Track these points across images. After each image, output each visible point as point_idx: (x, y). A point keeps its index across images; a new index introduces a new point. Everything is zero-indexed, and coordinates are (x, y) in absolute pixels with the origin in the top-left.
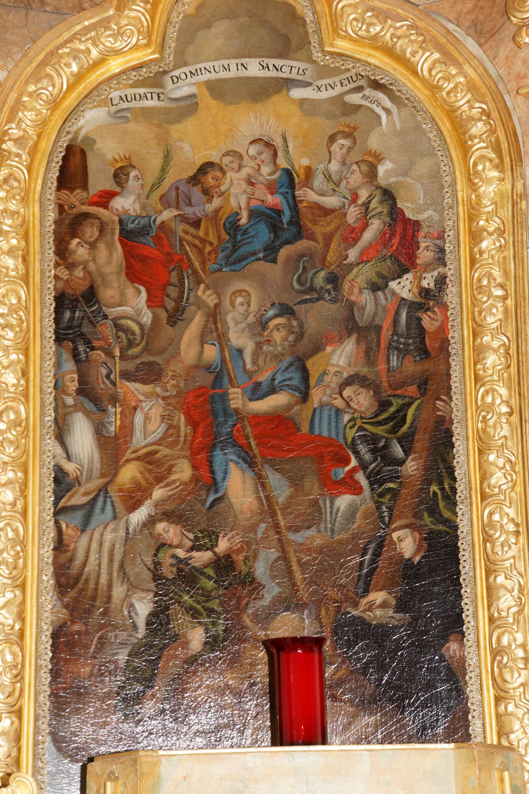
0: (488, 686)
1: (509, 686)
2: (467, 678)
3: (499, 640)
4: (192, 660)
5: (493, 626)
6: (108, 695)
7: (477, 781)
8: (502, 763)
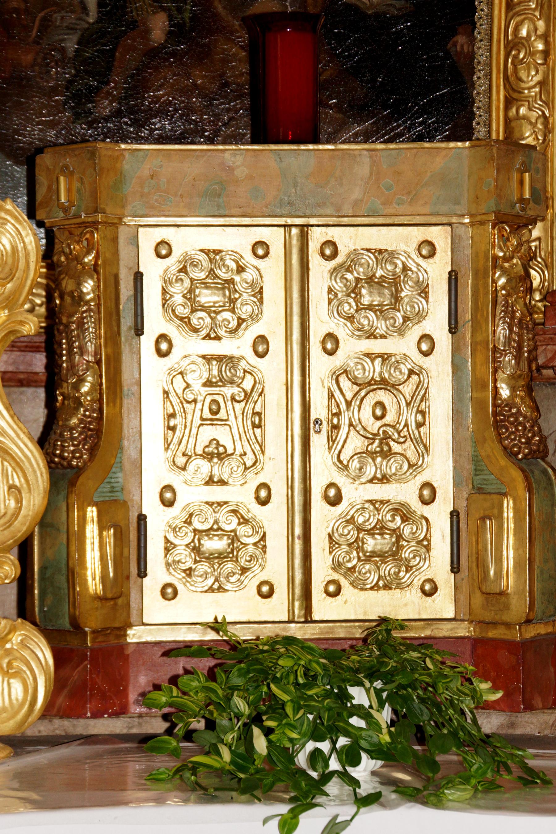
0: (498, 87)
1: (523, 85)
2: (475, 77)
3: (517, 29)
4: (154, 53)
5: (511, 14)
6: (54, 91)
7: (493, 184)
8: (523, 163)
